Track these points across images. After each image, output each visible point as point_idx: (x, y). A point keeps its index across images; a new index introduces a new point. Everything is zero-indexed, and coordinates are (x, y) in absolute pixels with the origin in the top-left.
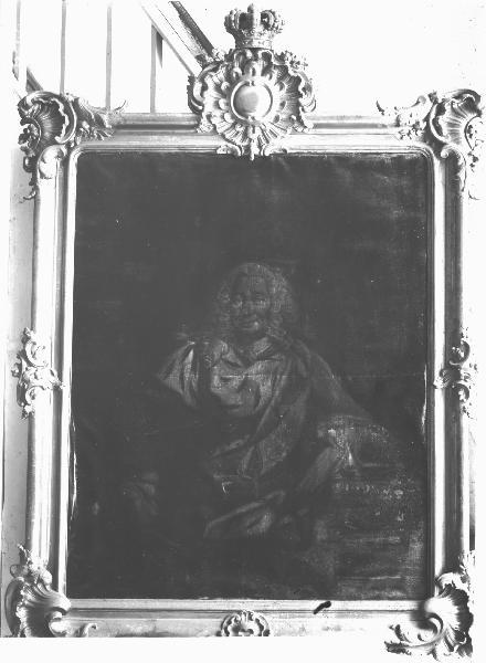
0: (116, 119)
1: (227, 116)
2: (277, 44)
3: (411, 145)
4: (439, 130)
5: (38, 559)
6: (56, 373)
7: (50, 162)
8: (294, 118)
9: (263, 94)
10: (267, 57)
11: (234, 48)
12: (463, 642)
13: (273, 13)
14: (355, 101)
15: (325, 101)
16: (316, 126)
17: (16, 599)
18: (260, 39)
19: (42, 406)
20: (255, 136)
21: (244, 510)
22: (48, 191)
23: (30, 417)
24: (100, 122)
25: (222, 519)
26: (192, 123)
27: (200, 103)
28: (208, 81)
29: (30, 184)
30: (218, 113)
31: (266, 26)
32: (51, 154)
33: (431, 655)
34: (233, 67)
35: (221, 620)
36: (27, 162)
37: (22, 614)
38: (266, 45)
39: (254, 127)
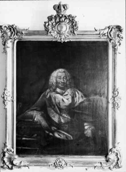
0: (26, 32)
1: (55, 32)
2: (67, 13)
3: (103, 39)
4: (110, 35)
5: (9, 146)
6: (12, 98)
7: (9, 44)
8: (72, 32)
9: (65, 28)
10: (65, 16)
11: (56, 14)
12: (117, 165)
13: (66, 6)
14: (89, 22)
15: (82, 26)
16: (78, 34)
17: (4, 155)
18: (63, 12)
19: (9, 106)
20: (63, 37)
21: (63, 132)
22: (9, 51)
23: (6, 109)
24: (22, 33)
25: (27, 139)
26: (46, 33)
27: (48, 29)
28: (50, 23)
29: (4, 49)
30: (52, 31)
31: (64, 8)
32: (9, 41)
33: (109, 169)
34: (57, 19)
35: (56, 159)
36: (3, 43)
37: (5, 159)
38: (64, 14)
39: (62, 35)
